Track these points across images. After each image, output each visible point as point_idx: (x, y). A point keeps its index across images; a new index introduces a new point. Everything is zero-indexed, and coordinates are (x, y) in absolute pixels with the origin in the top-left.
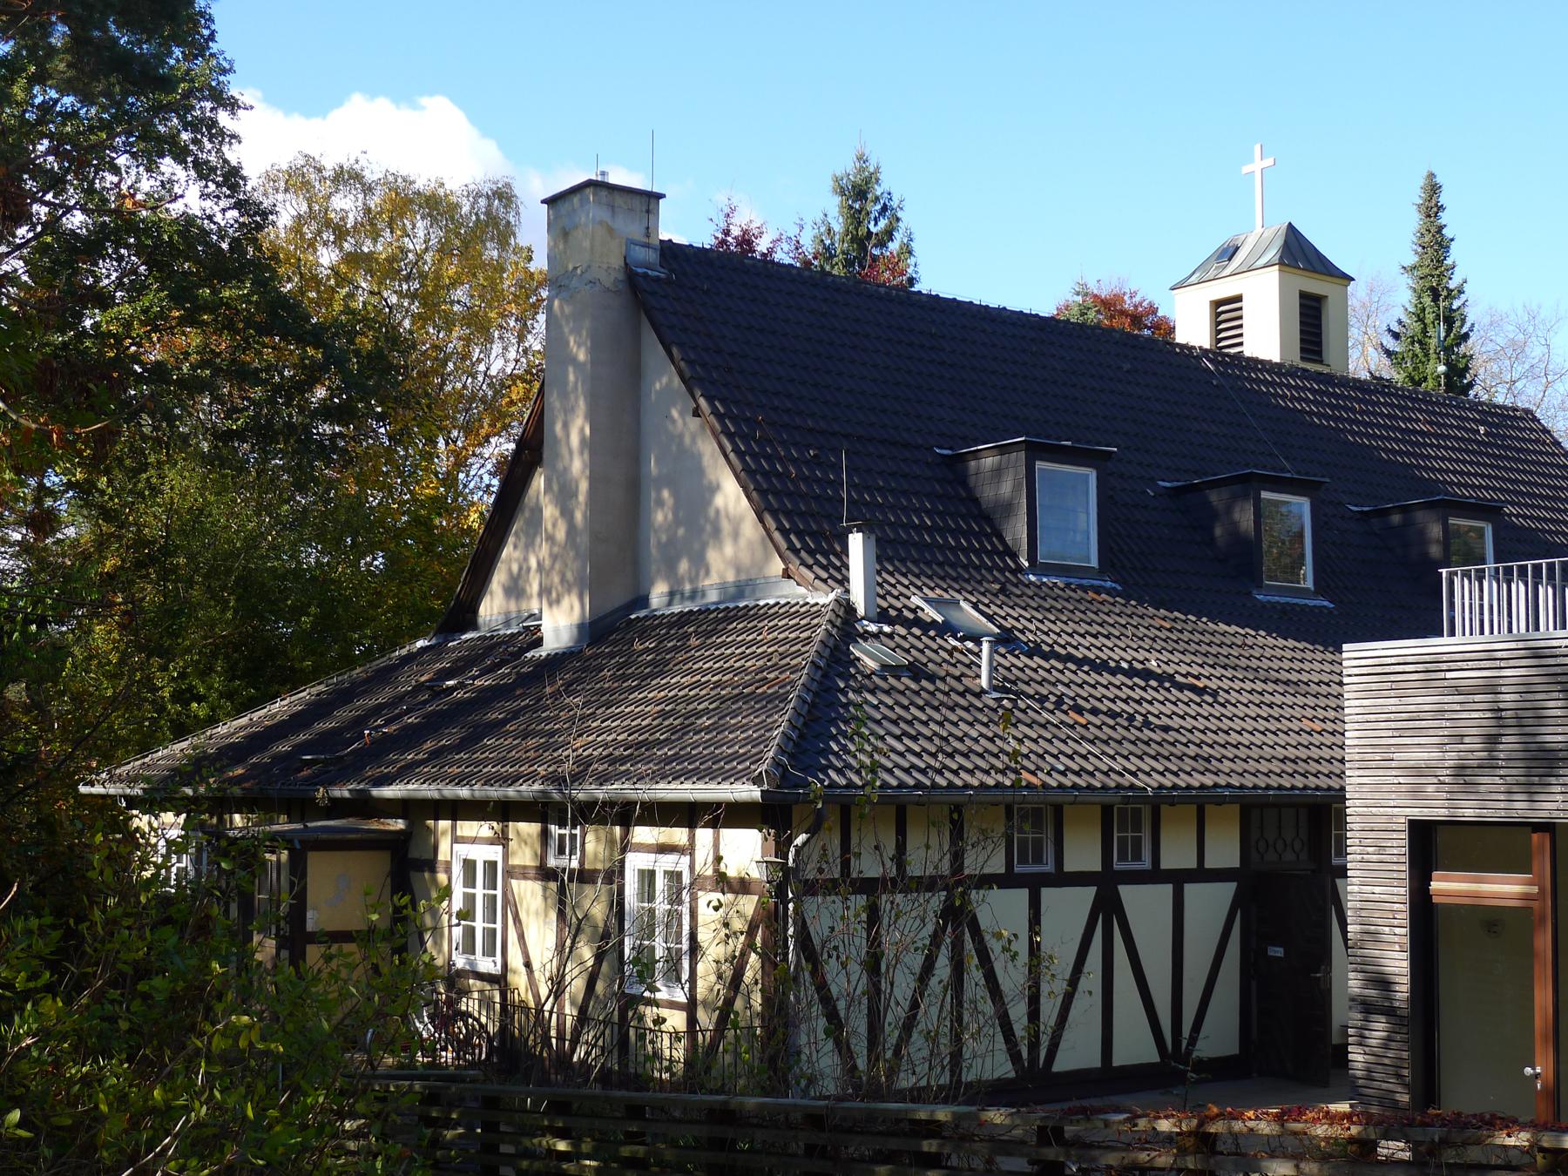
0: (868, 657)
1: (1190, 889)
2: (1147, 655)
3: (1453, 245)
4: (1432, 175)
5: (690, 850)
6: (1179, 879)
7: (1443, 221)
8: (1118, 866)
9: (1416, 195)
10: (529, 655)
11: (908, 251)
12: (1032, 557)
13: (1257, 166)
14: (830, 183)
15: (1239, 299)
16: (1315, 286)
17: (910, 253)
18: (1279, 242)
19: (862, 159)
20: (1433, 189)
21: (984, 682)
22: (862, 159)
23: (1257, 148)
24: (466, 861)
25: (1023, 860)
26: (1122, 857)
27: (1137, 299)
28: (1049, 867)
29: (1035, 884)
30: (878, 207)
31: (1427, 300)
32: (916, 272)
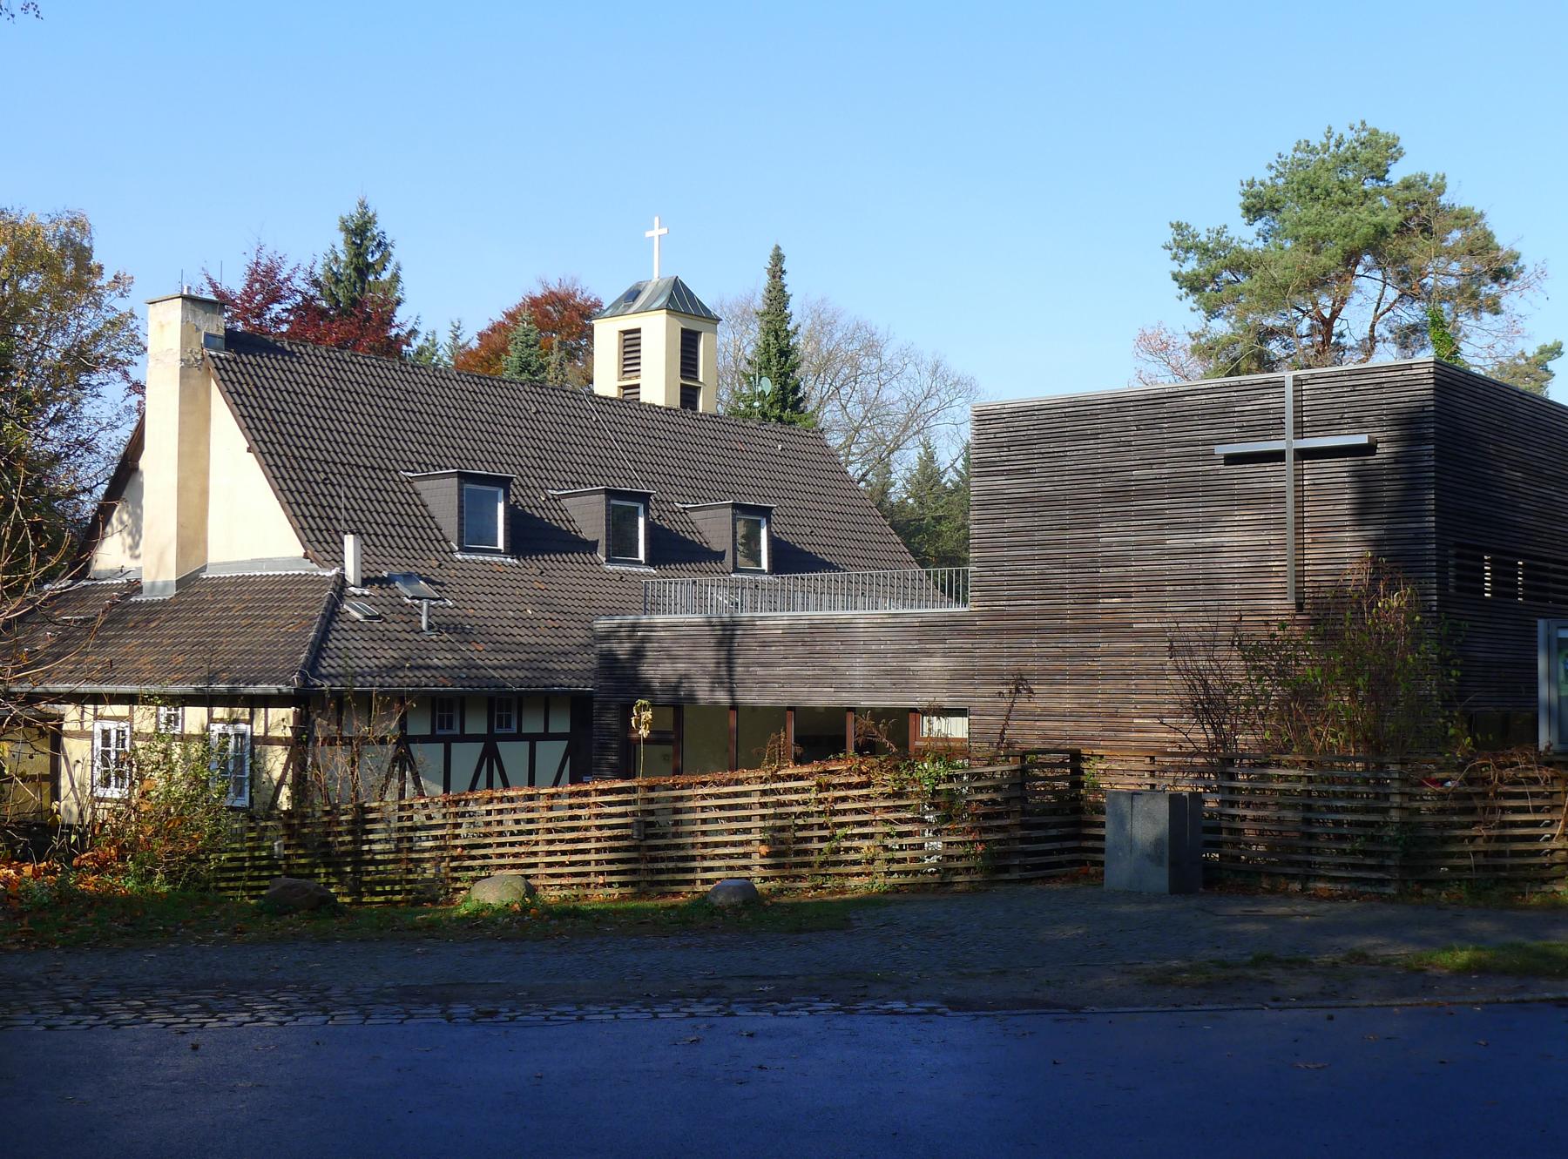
0: (353, 611)
1: (540, 745)
2: (526, 606)
3: (791, 299)
4: (778, 248)
5: (130, 719)
6: (533, 739)
7: (784, 282)
8: (497, 731)
9: (767, 262)
10: (133, 599)
11: (396, 278)
12: (460, 544)
13: (656, 232)
14: (337, 224)
15: (638, 331)
16: (693, 325)
17: (398, 281)
18: (668, 292)
19: (362, 205)
20: (778, 258)
21: (424, 626)
22: (362, 205)
23: (657, 219)
24: (104, 731)
25: (441, 727)
26: (500, 726)
27: (586, 295)
28: (457, 731)
29: (448, 741)
30: (375, 243)
31: (772, 340)
32: (403, 294)
